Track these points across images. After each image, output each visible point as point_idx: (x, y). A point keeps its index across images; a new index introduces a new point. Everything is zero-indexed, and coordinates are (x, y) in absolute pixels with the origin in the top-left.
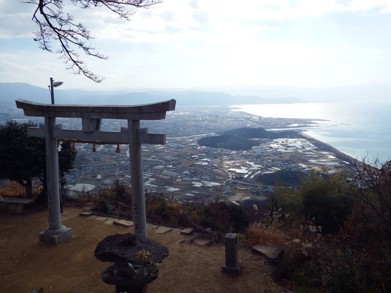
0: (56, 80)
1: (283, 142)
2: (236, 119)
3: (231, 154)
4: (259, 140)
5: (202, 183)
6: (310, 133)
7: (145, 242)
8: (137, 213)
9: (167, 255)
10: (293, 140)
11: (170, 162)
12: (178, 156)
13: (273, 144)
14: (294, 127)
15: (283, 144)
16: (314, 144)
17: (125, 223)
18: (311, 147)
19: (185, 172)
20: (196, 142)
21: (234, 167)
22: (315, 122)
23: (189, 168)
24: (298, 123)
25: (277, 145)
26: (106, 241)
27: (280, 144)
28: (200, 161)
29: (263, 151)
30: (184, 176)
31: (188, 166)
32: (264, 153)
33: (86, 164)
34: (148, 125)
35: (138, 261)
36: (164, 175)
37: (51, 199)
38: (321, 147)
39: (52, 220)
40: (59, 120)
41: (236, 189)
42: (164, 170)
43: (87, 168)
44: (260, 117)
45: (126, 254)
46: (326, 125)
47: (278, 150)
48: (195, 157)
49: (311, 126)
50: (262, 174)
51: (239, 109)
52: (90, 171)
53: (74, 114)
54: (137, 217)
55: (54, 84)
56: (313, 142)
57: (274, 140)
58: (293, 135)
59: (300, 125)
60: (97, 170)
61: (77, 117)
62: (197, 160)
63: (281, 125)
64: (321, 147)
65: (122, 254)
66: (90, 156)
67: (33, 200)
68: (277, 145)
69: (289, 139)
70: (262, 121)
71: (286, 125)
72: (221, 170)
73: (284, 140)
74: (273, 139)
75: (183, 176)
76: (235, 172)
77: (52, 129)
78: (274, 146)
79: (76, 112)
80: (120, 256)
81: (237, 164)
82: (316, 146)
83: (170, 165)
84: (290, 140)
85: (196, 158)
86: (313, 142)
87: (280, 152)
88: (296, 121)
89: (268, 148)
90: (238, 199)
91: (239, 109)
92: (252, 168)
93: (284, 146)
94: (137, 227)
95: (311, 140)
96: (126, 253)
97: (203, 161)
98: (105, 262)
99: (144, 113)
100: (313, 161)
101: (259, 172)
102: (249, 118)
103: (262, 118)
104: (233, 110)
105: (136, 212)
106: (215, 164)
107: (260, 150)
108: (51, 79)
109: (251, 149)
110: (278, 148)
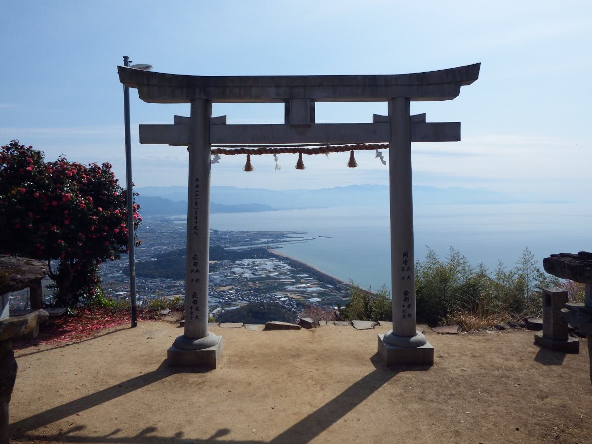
1: (249, 265)
3: (176, 286)
4: (215, 264)
6: (284, 250)
10: (262, 260)
13: (236, 267)
16: (289, 264)
22: (288, 235)
27: (245, 268)
29: (223, 278)
39: (197, 317)
40: (218, 110)
46: (302, 239)
47: (244, 276)
48: (121, 295)
49: (287, 241)
50: (223, 311)
57: (237, 262)
59: (269, 240)
67: (64, 309)
68: (242, 270)
69: (256, 260)
70: (219, 236)
73: (250, 261)
78: (238, 270)
84: (258, 261)
85: (123, 296)
87: (246, 278)
88: (263, 234)
89: (229, 274)
93: (250, 270)
94: (407, 296)
99: (429, 84)
100: (290, 288)
101: (219, 309)
103: (219, 231)
104: (176, 222)
105: (406, 269)
110: (243, 273)
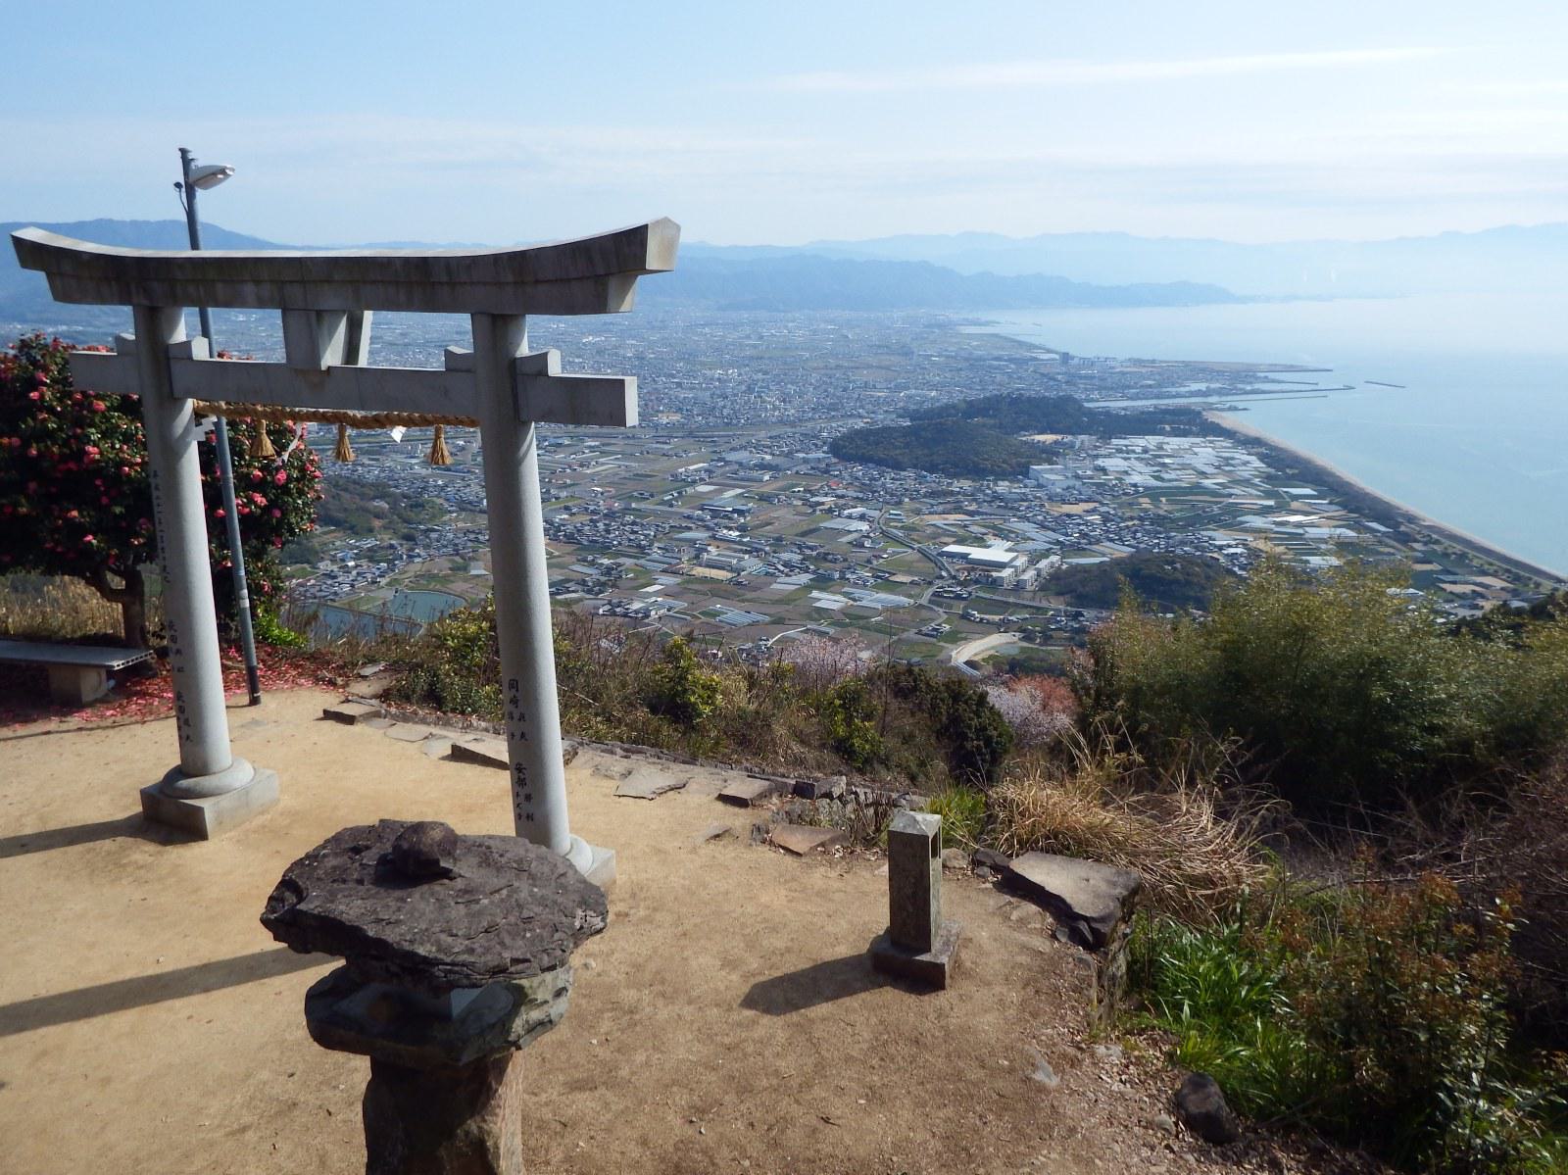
0: (202, 159)
2: (974, 363)
3: (952, 493)
4: (1056, 442)
5: (846, 595)
6: (1253, 417)
7: (503, 860)
8: (522, 718)
9: (601, 925)
11: (730, 519)
12: (760, 499)
13: (1109, 456)
14: (1193, 394)
15: (1147, 456)
16: (1262, 458)
17: (497, 752)
18: (1251, 464)
19: (786, 556)
20: (825, 448)
21: (961, 541)
22: (1271, 375)
23: (798, 540)
24: (1207, 381)
25: (1128, 463)
26: (325, 856)
28: (839, 516)
29: (1071, 482)
30: (782, 568)
31: (797, 535)
32: (1074, 488)
33: (430, 520)
34: (554, 342)
35: (448, 960)
36: (711, 565)
37: (178, 652)
38: (1288, 471)
39: (188, 738)
41: (969, 620)
42: (709, 548)
43: (434, 535)
44: (1066, 357)
45: (398, 922)
47: (1128, 480)
48: (823, 504)
51: (987, 324)
52: (446, 547)
53: (249, 289)
54: (523, 735)
55: (195, 179)
56: (1260, 450)
57: (1115, 441)
58: (1184, 424)
59: (1213, 386)
60: (470, 544)
61: (261, 304)
62: (830, 511)
63: (1142, 386)
64: (1287, 470)
65: (379, 921)
66: (443, 494)
68: (1128, 463)
69: (1167, 440)
70: (1072, 371)
71: (1160, 386)
72: (914, 549)
73: (1151, 441)
74: (1110, 439)
75: (777, 569)
76: (964, 556)
77: (168, 359)
79: (257, 282)
80: (371, 932)
81: (975, 529)
82: (1269, 466)
83: (730, 529)
84: (1173, 443)
85: (826, 507)
86: (1260, 450)
87: (1135, 485)
89: (1089, 473)
90: (976, 655)
91: (987, 324)
92: (1030, 545)
93: (1147, 464)
94: (522, 777)
95: (1251, 443)
96: (401, 921)
97: (850, 517)
98: (309, 952)
99: (537, 282)
102: (1021, 355)
105: (516, 716)
106: (896, 527)
107: (1061, 478)
108: (184, 152)
109: (1026, 475)
